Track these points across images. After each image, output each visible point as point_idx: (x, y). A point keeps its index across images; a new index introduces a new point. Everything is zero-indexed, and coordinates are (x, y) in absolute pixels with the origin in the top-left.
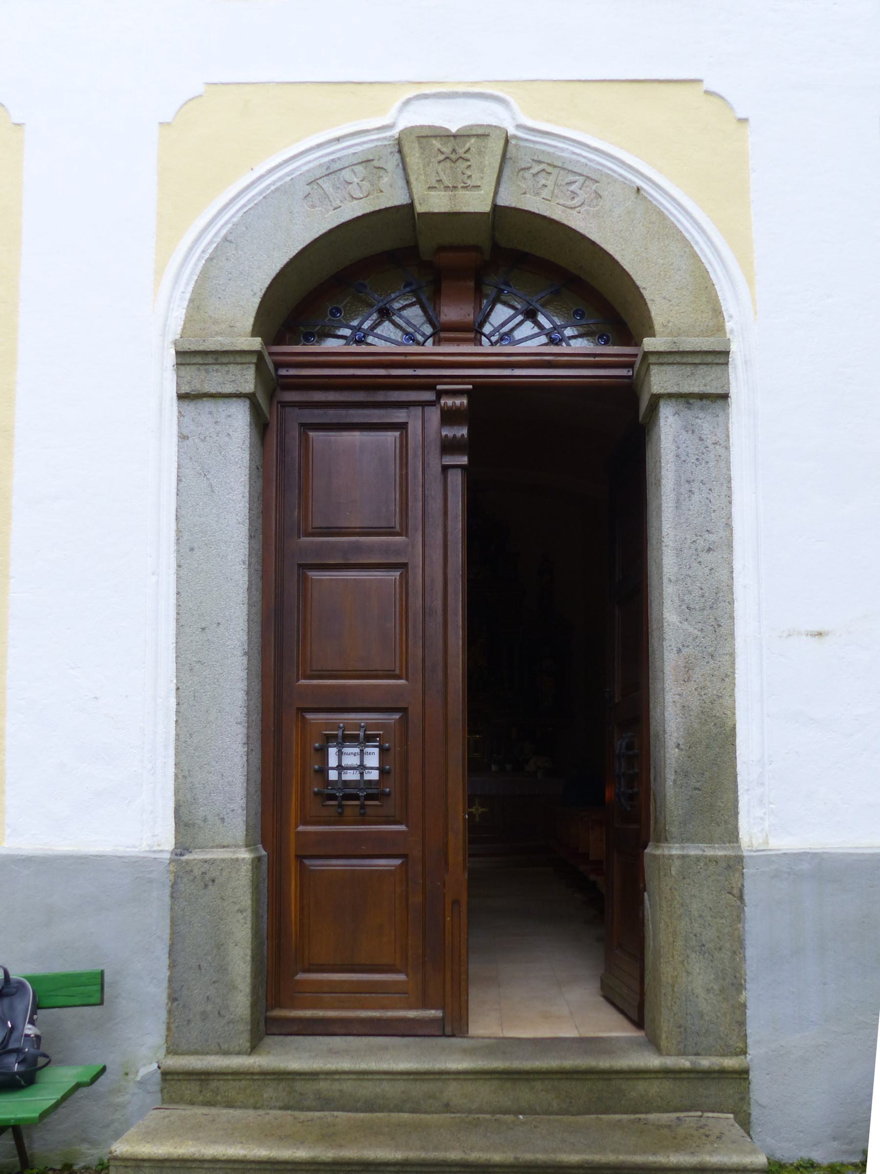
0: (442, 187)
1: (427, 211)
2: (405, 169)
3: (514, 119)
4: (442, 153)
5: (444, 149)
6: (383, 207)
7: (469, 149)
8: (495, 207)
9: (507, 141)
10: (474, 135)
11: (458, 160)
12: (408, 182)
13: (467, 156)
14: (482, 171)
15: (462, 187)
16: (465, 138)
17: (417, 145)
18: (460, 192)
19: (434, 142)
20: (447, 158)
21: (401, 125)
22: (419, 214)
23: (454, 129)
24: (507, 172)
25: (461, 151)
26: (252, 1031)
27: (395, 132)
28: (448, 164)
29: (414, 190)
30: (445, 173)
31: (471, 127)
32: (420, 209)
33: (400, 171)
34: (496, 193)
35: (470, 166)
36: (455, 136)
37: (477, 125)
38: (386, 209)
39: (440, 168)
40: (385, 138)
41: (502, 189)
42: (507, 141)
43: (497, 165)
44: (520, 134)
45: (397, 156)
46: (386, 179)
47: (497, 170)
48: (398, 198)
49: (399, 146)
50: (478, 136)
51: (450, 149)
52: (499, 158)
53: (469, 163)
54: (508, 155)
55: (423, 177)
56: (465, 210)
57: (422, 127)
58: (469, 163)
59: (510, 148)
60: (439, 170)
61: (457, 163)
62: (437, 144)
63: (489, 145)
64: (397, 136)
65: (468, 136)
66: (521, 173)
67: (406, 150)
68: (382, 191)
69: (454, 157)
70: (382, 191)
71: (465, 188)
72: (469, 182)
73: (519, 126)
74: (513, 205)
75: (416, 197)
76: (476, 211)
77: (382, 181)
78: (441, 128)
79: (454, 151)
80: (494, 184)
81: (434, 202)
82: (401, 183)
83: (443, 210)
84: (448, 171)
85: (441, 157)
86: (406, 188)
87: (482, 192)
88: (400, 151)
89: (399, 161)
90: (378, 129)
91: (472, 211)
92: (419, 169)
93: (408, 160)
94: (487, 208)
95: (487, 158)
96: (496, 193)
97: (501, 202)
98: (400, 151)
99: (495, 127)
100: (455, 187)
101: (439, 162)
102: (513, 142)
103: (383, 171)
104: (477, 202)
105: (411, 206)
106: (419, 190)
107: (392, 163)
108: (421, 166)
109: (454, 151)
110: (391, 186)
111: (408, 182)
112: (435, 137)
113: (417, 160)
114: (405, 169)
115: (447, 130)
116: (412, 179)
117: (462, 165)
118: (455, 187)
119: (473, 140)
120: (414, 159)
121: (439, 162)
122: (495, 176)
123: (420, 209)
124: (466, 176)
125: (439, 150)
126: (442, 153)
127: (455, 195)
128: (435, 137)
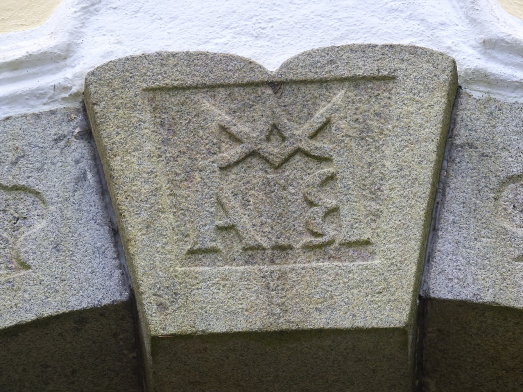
0: (237, 247)
1: (186, 329)
2: (105, 189)
3: (473, 21)
4: (236, 139)
5: (241, 128)
6: (30, 317)
7: (327, 124)
8: (425, 305)
9: (455, 92)
10: (342, 80)
11: (291, 156)
12: (116, 233)
13: (323, 145)
14: (375, 194)
15: (308, 248)
16: (314, 91)
17: (147, 116)
18: (301, 265)
19: (206, 104)
20: (253, 154)
21: (93, 54)
22: (155, 340)
23: (273, 62)
24: (459, 187)
25: (299, 131)
26: (52, 316)
27: (72, 75)
28: (256, 173)
29: (140, 263)
30: (245, 205)
31: (332, 54)
32: (159, 322)
33: (89, 198)
34: (426, 259)
35: (332, 178)
36: (276, 85)
37: (351, 49)
38: (41, 324)
39: (228, 186)
40: (37, 95)
41: (444, 245)
42: (455, 92)
43: (425, 173)
44: (496, 68)
45: (79, 149)
46: (39, 225)
47: (425, 190)
48: (90, 287)
49: (87, 117)
50: (355, 81)
51: (262, 126)
52: (430, 149)
53: (327, 170)
54: (462, 135)
55: (168, 219)
56: (319, 321)
57: (163, 58)
58: (327, 170)
59: (467, 111)
60: (227, 193)
61: (288, 171)
62: (215, 110)
63: (396, 110)
64: (78, 86)
65: (322, 82)
66: (508, 192)
67: (110, 132)
68: (25, 266)
69: (274, 149)
70: (25, 266)
71: (320, 248)
72: (330, 231)
73: (491, 45)
74: (487, 297)
75: (146, 284)
76: (360, 323)
77: (25, 233)
78: (230, 58)
79: (275, 131)
80: (417, 232)
81: (208, 298)
82: (93, 235)
83: (241, 325)
84: (256, 196)
85: (232, 152)
86: (111, 252)
87: (377, 261)
88: (88, 134)
89: (86, 164)
90: (15, 65)
91: (346, 324)
92: (154, 193)
93: (116, 163)
94: (394, 312)
95: (388, 151)
96: (426, 259)
97: (441, 289)
98: (88, 134)
99: (414, 50)
100: (283, 249)
101: (225, 168)
102: (476, 92)
103: (31, 199)
104: (365, 294)
105: (129, 310)
106: (156, 262)
107: (62, 171)
108: (163, 182)
109: (275, 131)
110: (57, 247)
111: (116, 233)
112: (210, 88)
113: (147, 166)
114: (105, 189)
115: (249, 65)
116: (133, 225)
117: (305, 176)
118: (283, 249)
119: (339, 96)
120: (139, 161)
121: (225, 168)
122: (420, 208)
123: (159, 322)
124: (319, 211)
125: (223, 129)
126: (236, 139)
127: (283, 275)
128: (210, 88)
